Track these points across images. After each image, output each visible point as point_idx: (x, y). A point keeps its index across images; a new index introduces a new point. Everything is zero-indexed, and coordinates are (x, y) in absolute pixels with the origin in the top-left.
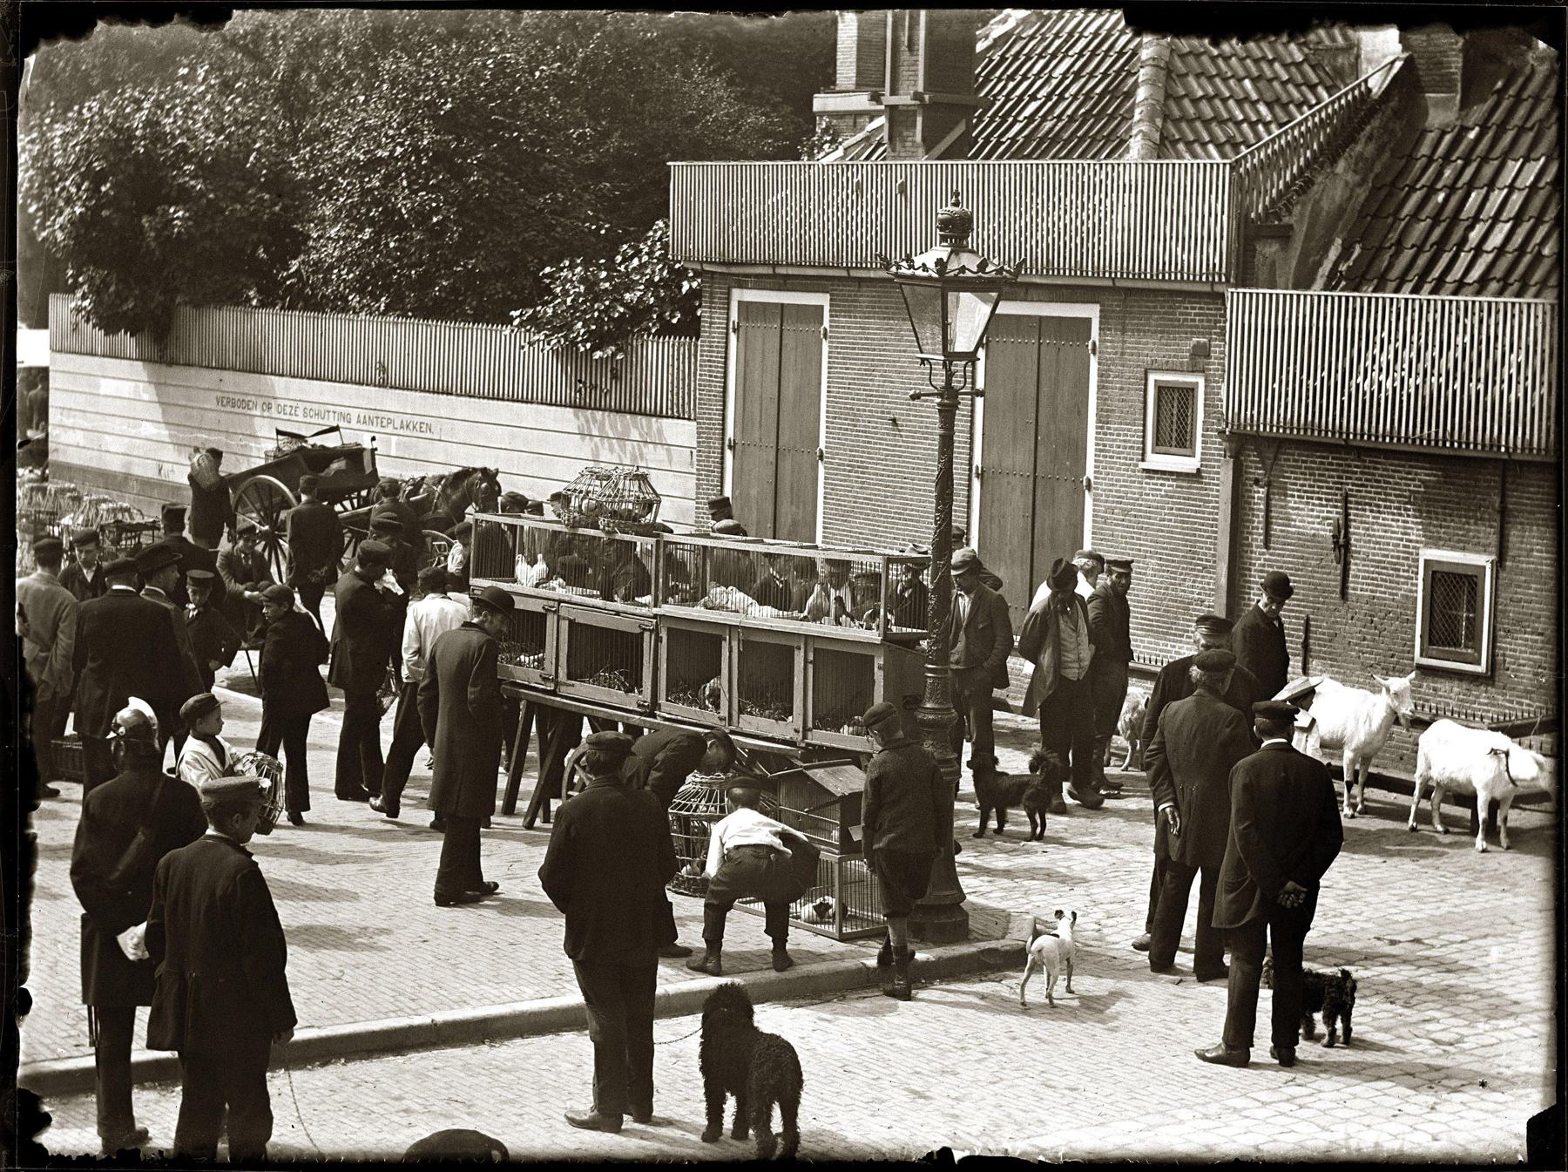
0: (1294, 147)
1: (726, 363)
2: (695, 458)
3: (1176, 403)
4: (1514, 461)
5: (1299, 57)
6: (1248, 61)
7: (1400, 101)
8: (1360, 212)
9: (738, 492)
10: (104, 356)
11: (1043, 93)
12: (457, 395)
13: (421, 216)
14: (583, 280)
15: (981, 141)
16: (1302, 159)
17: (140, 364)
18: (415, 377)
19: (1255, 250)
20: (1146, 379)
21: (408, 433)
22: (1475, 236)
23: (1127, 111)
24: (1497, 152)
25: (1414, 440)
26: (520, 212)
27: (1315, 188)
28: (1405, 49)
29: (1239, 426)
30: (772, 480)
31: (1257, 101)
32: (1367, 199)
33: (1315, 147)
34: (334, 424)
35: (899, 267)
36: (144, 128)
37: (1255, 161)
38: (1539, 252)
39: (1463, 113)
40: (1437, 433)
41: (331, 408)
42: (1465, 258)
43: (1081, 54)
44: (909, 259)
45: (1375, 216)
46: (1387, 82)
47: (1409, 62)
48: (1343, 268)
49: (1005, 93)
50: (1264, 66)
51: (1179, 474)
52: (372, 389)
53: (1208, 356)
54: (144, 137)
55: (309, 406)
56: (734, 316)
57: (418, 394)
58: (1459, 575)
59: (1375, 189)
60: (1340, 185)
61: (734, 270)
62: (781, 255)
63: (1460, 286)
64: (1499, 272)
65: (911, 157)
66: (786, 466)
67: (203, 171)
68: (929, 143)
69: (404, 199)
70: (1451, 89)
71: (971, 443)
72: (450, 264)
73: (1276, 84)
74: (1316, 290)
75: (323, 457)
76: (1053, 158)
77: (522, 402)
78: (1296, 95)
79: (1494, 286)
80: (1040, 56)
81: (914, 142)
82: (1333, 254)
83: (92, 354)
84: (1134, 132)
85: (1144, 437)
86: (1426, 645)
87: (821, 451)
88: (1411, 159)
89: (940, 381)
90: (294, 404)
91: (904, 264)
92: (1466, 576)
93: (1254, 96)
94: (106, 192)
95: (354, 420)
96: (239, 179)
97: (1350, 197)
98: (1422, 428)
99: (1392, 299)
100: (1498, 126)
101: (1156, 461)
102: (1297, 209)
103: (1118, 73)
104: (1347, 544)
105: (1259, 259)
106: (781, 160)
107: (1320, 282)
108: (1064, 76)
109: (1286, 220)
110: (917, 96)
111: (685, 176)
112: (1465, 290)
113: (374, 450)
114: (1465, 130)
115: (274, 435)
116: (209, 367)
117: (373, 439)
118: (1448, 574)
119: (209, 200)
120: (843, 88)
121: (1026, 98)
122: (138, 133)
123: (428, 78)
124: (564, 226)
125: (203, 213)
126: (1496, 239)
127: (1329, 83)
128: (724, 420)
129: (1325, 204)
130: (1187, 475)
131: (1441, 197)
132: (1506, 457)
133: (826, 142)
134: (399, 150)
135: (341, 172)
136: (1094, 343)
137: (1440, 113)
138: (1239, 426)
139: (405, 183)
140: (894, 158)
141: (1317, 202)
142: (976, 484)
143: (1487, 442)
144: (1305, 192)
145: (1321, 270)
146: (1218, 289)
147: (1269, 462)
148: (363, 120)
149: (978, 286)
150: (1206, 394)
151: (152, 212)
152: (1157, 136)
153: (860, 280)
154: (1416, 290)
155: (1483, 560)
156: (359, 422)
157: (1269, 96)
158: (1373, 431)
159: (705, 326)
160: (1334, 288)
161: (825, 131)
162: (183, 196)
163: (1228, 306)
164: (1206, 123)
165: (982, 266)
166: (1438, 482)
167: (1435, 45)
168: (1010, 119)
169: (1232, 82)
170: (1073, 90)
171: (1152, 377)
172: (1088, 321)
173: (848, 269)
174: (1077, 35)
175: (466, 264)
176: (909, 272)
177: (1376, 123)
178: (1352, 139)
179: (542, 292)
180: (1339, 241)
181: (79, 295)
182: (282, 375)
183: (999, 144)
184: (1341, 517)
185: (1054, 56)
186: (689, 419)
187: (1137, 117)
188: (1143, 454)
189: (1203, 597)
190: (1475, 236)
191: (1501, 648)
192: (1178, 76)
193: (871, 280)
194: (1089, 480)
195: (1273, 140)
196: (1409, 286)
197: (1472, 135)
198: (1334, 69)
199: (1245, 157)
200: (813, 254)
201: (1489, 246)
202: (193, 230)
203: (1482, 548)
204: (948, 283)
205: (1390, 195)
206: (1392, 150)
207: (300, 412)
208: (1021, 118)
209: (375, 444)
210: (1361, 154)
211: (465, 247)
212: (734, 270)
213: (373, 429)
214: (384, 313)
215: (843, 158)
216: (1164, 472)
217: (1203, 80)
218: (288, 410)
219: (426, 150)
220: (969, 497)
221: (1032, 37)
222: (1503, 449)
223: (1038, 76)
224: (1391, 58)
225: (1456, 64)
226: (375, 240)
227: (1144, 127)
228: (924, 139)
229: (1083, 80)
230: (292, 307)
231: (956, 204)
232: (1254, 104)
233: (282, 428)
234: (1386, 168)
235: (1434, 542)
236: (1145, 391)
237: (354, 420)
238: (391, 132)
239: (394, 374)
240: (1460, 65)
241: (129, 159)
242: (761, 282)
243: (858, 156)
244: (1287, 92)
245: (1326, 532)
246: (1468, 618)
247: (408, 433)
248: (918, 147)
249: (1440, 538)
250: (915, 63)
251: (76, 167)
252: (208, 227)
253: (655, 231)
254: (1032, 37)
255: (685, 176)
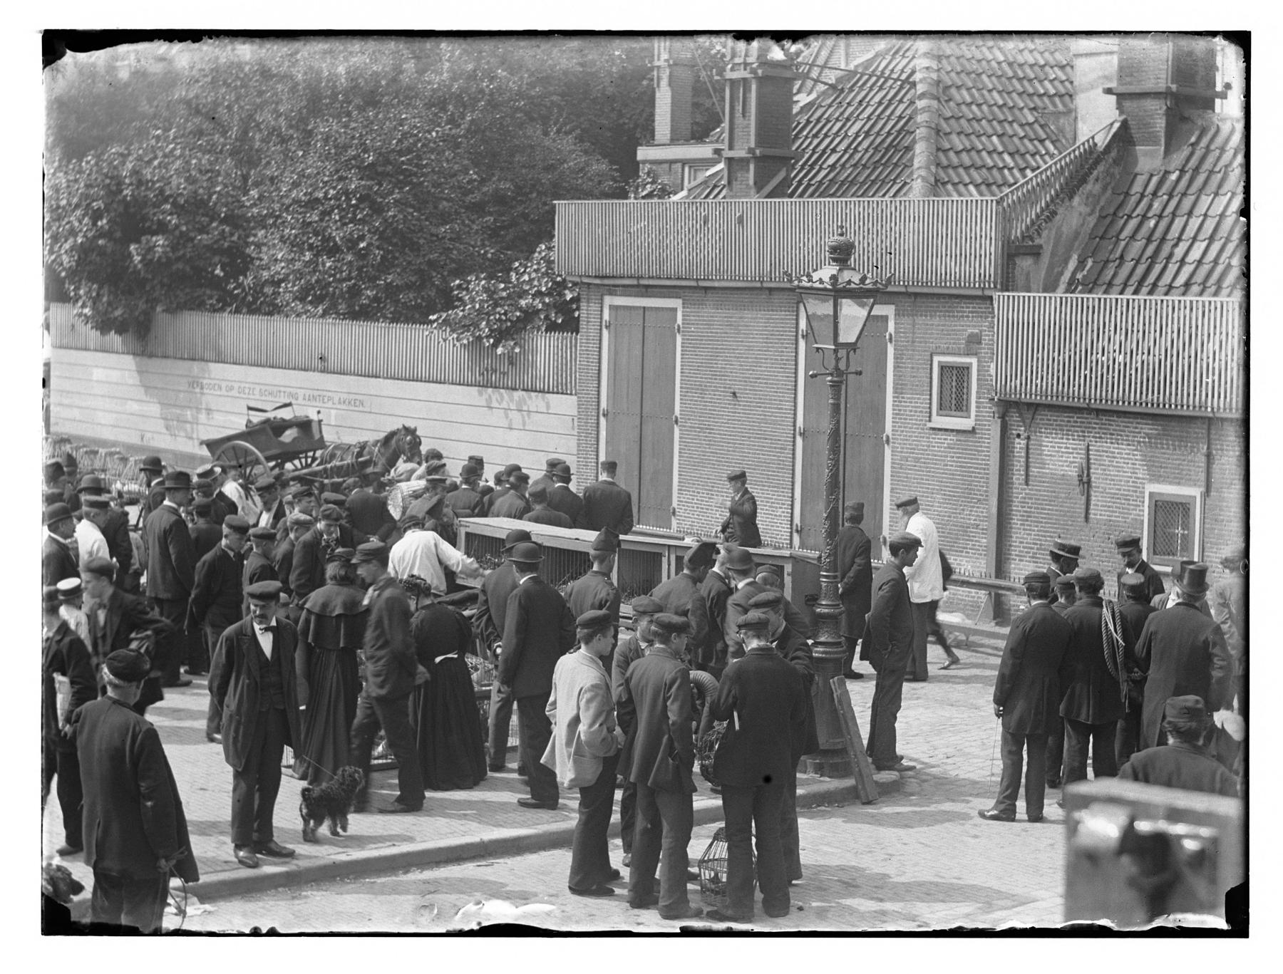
0: (1044, 185)
1: (600, 352)
2: (576, 423)
3: (955, 378)
4: (1217, 418)
5: (1031, 119)
6: (995, 123)
7: (1118, 151)
8: (1090, 234)
9: (610, 449)
10: (96, 350)
11: (842, 147)
12: (384, 378)
13: (352, 243)
14: (486, 290)
15: (795, 183)
16: (1048, 196)
17: (131, 357)
18: (350, 364)
19: (1015, 264)
20: (932, 361)
21: (344, 407)
22: (1179, 252)
23: (908, 160)
24: (1194, 189)
25: (1141, 404)
26: (425, 239)
27: (1058, 217)
28: (1121, 113)
29: (1005, 394)
30: (638, 439)
31: (1003, 152)
32: (1096, 225)
33: (1057, 187)
34: (288, 401)
35: (800, 281)
36: (131, 176)
37: (1015, 197)
38: (1229, 264)
39: (1166, 160)
40: (1158, 398)
41: (282, 389)
42: (1172, 268)
43: (869, 118)
44: (809, 276)
45: (1102, 238)
46: (1109, 138)
47: (1125, 125)
48: (1079, 276)
49: (811, 147)
50: (1006, 125)
51: (958, 431)
52: (316, 373)
53: (980, 343)
54: (131, 184)
55: (264, 388)
56: (606, 316)
57: (352, 377)
58: (1176, 503)
59: (1102, 218)
60: (1076, 215)
61: (606, 282)
62: (644, 270)
63: (1170, 289)
64: (1199, 277)
65: (745, 196)
66: (648, 429)
67: (179, 209)
68: (759, 186)
69: (337, 229)
70: (1156, 143)
71: (795, 410)
72: (373, 279)
73: (1015, 139)
74: (1059, 294)
75: (278, 427)
76: (852, 196)
77: (436, 382)
78: (1030, 147)
79: (1195, 289)
80: (837, 120)
81: (748, 185)
82: (1072, 264)
83: (86, 349)
84: (915, 176)
85: (930, 404)
86: (1151, 555)
87: (676, 418)
88: (1127, 194)
89: (831, 364)
90: (252, 386)
91: (805, 278)
92: (1181, 503)
93: (1000, 149)
94: (102, 227)
95: (301, 398)
96: (203, 215)
97: (1082, 225)
98: (1147, 394)
99: (1117, 300)
100: (1194, 170)
101: (940, 421)
102: (1045, 234)
103: (899, 132)
104: (1089, 482)
105: (1017, 272)
106: (618, 198)
107: (1062, 287)
108: (857, 135)
109: (1038, 241)
110: (751, 150)
111: (566, 210)
112: (1173, 291)
113: (320, 421)
114: (1167, 173)
115: (245, 410)
116: (182, 359)
117: (319, 412)
118: (1167, 502)
119: (181, 232)
120: (662, 142)
121: (829, 151)
122: (127, 181)
123: (353, 138)
124: (458, 250)
125: (179, 241)
126: (1195, 254)
127: (1054, 138)
128: (599, 395)
129: (1064, 229)
130: (964, 432)
131: (1152, 223)
132: (1211, 415)
133: (648, 183)
134: (332, 192)
135: (287, 210)
136: (891, 335)
137: (1148, 159)
138: (1005, 394)
139: (337, 218)
140: (732, 197)
141: (1059, 228)
142: (799, 441)
143: (1197, 404)
144: (1050, 220)
145: (1063, 278)
146: (987, 293)
147: (1028, 421)
148: (303, 170)
149: (857, 294)
150: (978, 371)
151: (138, 241)
152: (932, 180)
153: (706, 288)
154: (1136, 292)
155: (1195, 492)
156: (304, 399)
157: (1012, 149)
158: (1109, 397)
159: (583, 324)
160: (1073, 292)
161: (648, 174)
162: (162, 228)
163: (996, 306)
164: (967, 168)
165: (863, 279)
166: (1159, 434)
167: (1145, 111)
168: (817, 167)
169: (984, 138)
170: (865, 144)
171: (936, 359)
172: (675, 310)
173: (697, 280)
174: (865, 105)
175: (386, 278)
176: (809, 285)
177: (1101, 168)
178: (1083, 181)
179: (449, 301)
180: (1075, 257)
181: (80, 303)
182: (242, 364)
183: (809, 185)
184: (1084, 462)
185: (848, 119)
186: (571, 394)
187: (916, 163)
188: (930, 417)
189: (978, 522)
190: (1179, 252)
191: (1208, 556)
192: (946, 134)
193: (714, 288)
194: (888, 437)
195: (1027, 183)
196: (1131, 289)
197: (1174, 177)
198: (1058, 128)
199: (1007, 195)
200: (670, 269)
201: (1190, 259)
202: (171, 254)
203: (1192, 483)
204: (838, 292)
205: (1112, 222)
206: (1113, 189)
207: (257, 392)
208: (825, 166)
209: (321, 417)
210: (1091, 191)
211: (385, 265)
212: (606, 282)
213: (317, 404)
214: (323, 316)
215: (687, 197)
216: (946, 430)
217: (963, 137)
218: (247, 391)
219: (354, 192)
220: (794, 450)
221: (830, 106)
222: (1209, 409)
223: (837, 134)
224: (1111, 121)
225: (1160, 124)
226: (313, 262)
227: (923, 172)
228: (755, 183)
229: (872, 138)
230: (237, 311)
231: (842, 235)
232: (1000, 154)
233: (252, 404)
234: (1109, 202)
235: (1156, 478)
236: (931, 369)
237: (301, 398)
238: (326, 179)
239: (333, 362)
240: (1163, 125)
241: (119, 201)
242: (627, 290)
243: (699, 195)
244: (1024, 145)
245: (1073, 472)
246: (1183, 535)
247: (344, 407)
248: (750, 188)
249: (1160, 476)
250: (748, 126)
251: (77, 206)
252: (181, 252)
253: (540, 253)
254: (830, 106)
255: (566, 210)
